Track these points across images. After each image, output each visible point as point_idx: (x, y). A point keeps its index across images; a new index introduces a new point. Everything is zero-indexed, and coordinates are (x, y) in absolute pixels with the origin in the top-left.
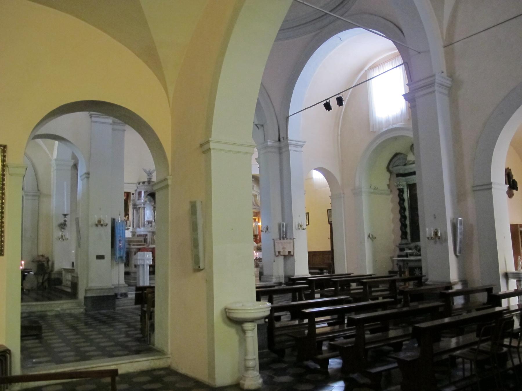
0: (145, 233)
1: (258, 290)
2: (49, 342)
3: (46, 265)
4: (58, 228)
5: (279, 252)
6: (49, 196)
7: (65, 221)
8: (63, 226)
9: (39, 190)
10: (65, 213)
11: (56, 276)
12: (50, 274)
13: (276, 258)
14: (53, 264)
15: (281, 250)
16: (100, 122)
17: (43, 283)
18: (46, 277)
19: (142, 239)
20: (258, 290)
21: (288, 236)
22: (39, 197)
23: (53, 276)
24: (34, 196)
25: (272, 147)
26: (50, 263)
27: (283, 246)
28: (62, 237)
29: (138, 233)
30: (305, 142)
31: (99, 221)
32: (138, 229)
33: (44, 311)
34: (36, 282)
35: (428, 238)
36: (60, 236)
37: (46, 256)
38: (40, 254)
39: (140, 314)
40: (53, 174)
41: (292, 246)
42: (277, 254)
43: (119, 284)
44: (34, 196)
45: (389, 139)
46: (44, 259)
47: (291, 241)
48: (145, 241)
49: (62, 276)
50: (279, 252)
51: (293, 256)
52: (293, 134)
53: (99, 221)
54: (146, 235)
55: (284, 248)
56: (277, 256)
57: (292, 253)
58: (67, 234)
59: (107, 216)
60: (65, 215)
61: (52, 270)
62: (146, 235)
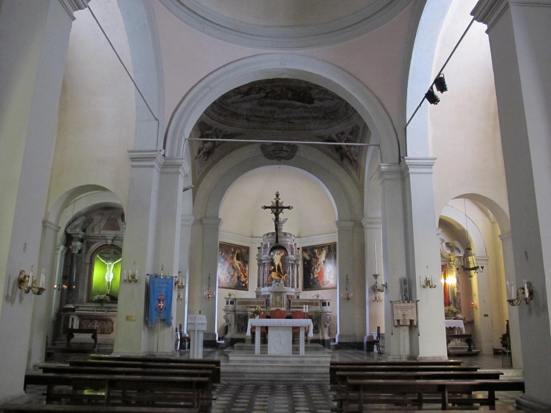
0: (267, 293)
1: (333, 366)
2: (306, 404)
5: (398, 321)
13: (395, 330)
15: (401, 318)
16: (140, 166)
19: (263, 300)
20: (333, 366)
21: (413, 299)
25: (388, 172)
27: (405, 312)
29: (263, 294)
30: (435, 159)
31: (133, 277)
32: (262, 289)
33: (243, 373)
35: (125, 280)
41: (415, 312)
42: (396, 323)
43: (413, 356)
47: (414, 305)
48: (267, 302)
50: (398, 321)
51: (417, 326)
52: (414, 149)
53: (133, 277)
54: (269, 296)
55: (404, 315)
56: (396, 326)
57: (415, 323)
59: (130, 271)
62: (269, 296)
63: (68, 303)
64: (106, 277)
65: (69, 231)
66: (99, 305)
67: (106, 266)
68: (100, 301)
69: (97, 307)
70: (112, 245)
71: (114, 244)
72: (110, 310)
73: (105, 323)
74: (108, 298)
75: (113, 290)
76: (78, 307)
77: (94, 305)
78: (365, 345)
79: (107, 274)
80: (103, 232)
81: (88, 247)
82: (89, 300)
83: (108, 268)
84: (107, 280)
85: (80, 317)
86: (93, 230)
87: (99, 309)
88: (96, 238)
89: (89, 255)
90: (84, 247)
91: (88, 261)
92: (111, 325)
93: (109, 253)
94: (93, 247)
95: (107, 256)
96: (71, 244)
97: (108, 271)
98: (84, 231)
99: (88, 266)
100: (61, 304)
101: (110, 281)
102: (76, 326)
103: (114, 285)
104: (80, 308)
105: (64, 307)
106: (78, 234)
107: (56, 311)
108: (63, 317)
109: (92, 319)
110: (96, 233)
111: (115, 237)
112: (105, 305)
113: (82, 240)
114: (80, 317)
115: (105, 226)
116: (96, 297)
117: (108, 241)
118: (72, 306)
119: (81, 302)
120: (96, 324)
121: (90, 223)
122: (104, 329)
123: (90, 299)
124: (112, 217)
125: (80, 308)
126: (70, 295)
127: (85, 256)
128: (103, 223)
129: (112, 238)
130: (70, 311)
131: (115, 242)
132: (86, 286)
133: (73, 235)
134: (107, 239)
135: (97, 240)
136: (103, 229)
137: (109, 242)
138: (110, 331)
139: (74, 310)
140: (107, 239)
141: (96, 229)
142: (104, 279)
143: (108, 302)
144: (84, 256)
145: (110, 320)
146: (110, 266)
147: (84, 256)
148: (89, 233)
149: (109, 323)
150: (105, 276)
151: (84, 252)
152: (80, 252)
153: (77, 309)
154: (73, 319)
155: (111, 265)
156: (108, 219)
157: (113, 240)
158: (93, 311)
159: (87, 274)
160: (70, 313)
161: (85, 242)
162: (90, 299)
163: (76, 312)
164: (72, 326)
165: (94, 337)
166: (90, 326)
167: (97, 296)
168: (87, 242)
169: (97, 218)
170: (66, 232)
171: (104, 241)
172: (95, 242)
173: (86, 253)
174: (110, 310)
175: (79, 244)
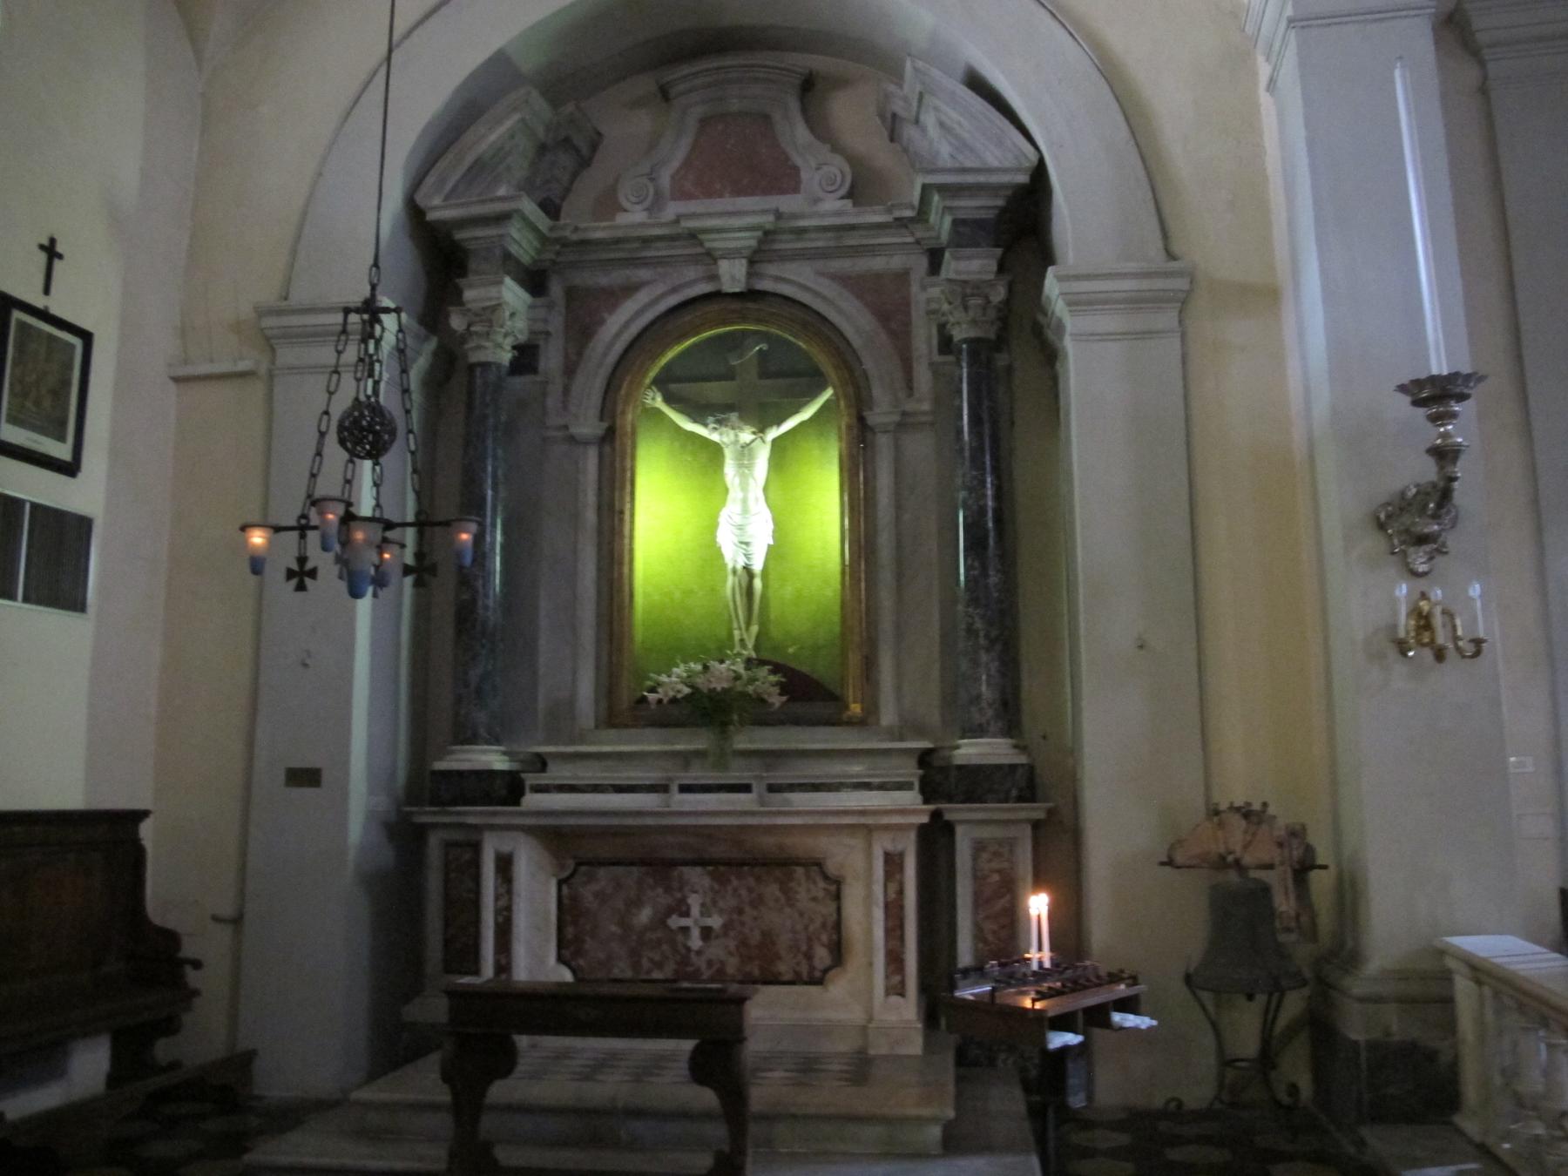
3: (1284, 903)
4: (1374, 543)
6: (1263, 296)
7: (1444, 454)
8: (1416, 522)
9: (1171, 256)
10: (1438, 366)
11: (1396, 1025)
12: (1324, 990)
14: (1350, 894)
17: (1267, 1058)
18: (1294, 1004)
22: (1183, 302)
23: (1356, 1028)
24: (1136, 302)
26: (1320, 882)
28: (1424, 623)
34: (1205, 1061)
36: (1405, 624)
37: (1283, 815)
38: (1235, 791)
39: (1478, 35)
40: (1280, 124)
44: (1136, 302)
45: (653, 323)
46: (1264, 851)
49: (1450, 1026)
58: (1473, 596)
60: (1436, 395)
61: (1344, 953)
63: (466, 735)
64: (726, 540)
65: (440, 210)
66: (696, 741)
67: (714, 453)
68: (709, 709)
69: (686, 759)
70: (751, 294)
71: (765, 285)
72: (782, 776)
73: (772, 890)
74: (766, 683)
75: (775, 632)
76: (541, 763)
77: (650, 742)
78: (932, 807)
79: (729, 513)
80: (672, 209)
81: (581, 330)
82: (627, 708)
83: (730, 467)
84: (733, 557)
85: (558, 838)
86: (608, 204)
87: (696, 775)
88: (634, 252)
89: (591, 383)
90: (556, 323)
91: (588, 426)
92: (829, 909)
93: (729, 375)
94: (620, 324)
95: (715, 391)
96: (457, 299)
97: (735, 493)
98: (551, 209)
99: (591, 460)
100: (421, 744)
101: (757, 567)
102: (536, 961)
103: (784, 594)
104: (558, 773)
105: (441, 765)
106: (501, 218)
107: (383, 803)
108: (434, 840)
109: (655, 857)
110: (633, 217)
111: (768, 235)
112: (746, 739)
113: (535, 281)
114: (558, 838)
115: (687, 164)
116: (674, 680)
117: (724, 266)
118: (494, 759)
119: (561, 719)
120: (694, 902)
121: (584, 163)
122: (768, 938)
123: (625, 698)
124: (735, 105)
125: (558, 773)
126: (474, 674)
127: (566, 390)
128: (676, 152)
129: (748, 241)
130: (488, 799)
131: (772, 269)
132: (588, 613)
133: (459, 235)
134: (711, 257)
135: (644, 274)
136: (681, 194)
137: (733, 275)
138: (822, 955)
139: (509, 789)
140: (711, 257)
141: (625, 196)
142: (714, 554)
143: (763, 717)
144: (555, 389)
145: (816, 865)
146: (745, 452)
147: (555, 389)
148: (580, 221)
149: (807, 890)
150: (713, 527)
151: (551, 359)
152: (526, 358)
153: (530, 779)
154: (505, 865)
155: (747, 451)
156: (704, 122)
157: (755, 259)
158: (660, 788)
159: (590, 516)
160: (474, 815)
161: (556, 289)
162: (625, 698)
163: (531, 800)
164: (504, 967)
165: (719, 1061)
166: (645, 915)
167: (680, 670)
168: (571, 293)
169: (625, 125)
170: (414, 211)
171: (691, 273)
172: (630, 290)
173: (570, 370)
174: (782, 776)
175: (512, 294)
